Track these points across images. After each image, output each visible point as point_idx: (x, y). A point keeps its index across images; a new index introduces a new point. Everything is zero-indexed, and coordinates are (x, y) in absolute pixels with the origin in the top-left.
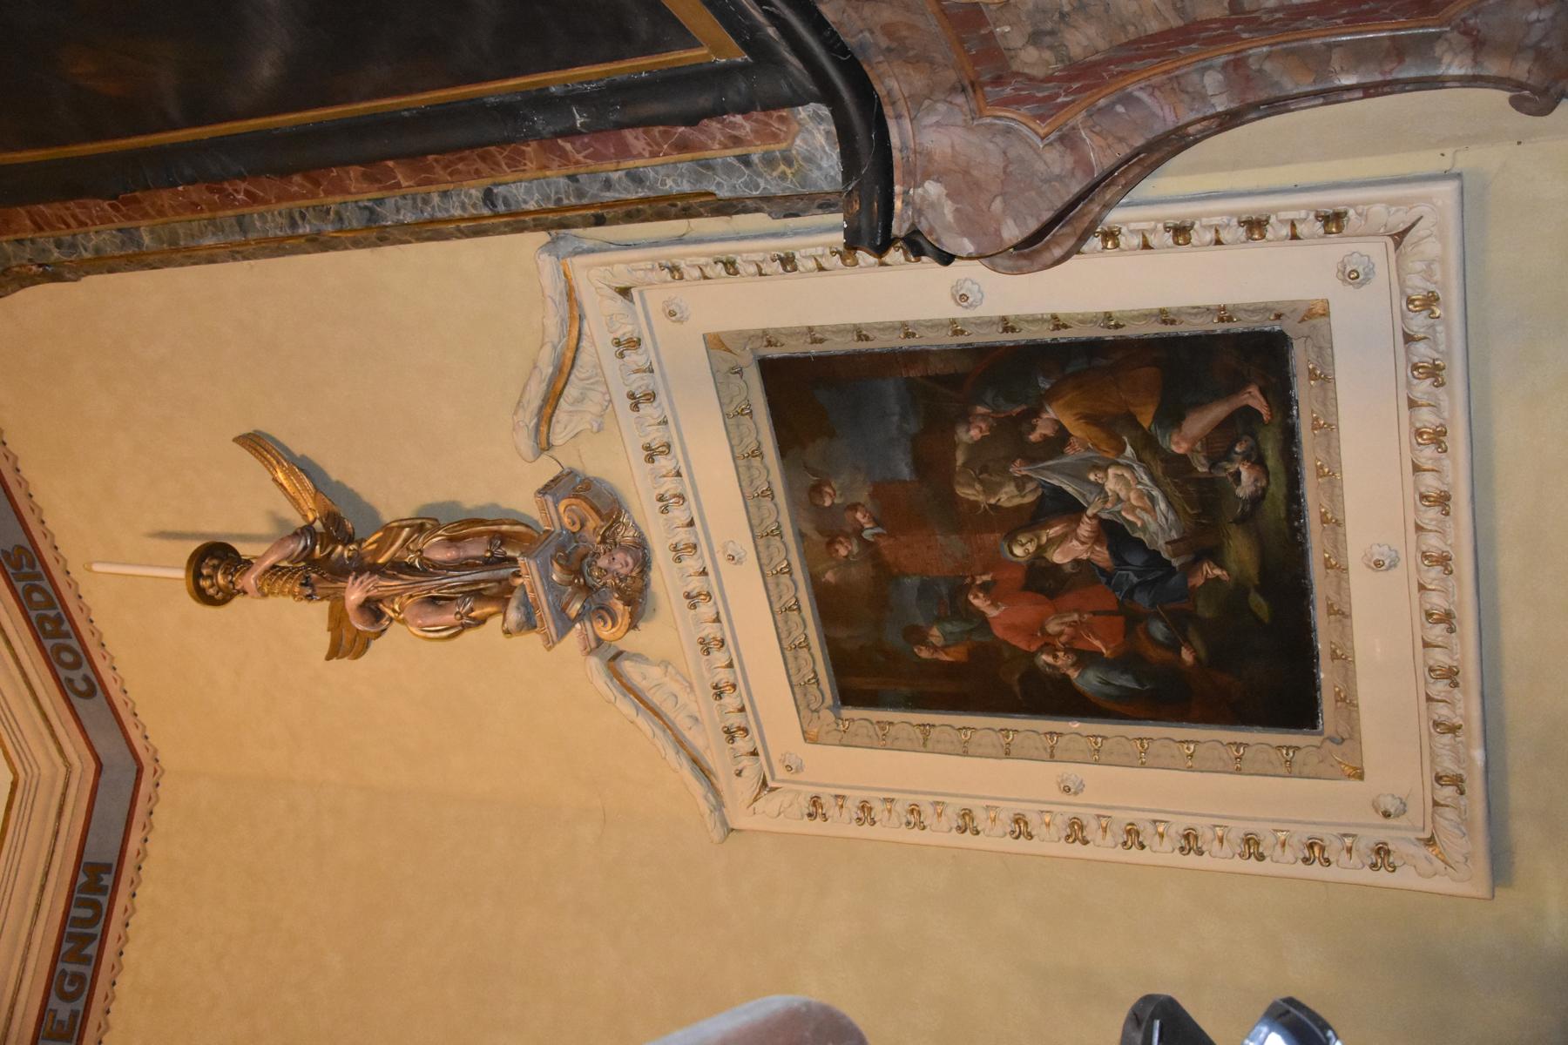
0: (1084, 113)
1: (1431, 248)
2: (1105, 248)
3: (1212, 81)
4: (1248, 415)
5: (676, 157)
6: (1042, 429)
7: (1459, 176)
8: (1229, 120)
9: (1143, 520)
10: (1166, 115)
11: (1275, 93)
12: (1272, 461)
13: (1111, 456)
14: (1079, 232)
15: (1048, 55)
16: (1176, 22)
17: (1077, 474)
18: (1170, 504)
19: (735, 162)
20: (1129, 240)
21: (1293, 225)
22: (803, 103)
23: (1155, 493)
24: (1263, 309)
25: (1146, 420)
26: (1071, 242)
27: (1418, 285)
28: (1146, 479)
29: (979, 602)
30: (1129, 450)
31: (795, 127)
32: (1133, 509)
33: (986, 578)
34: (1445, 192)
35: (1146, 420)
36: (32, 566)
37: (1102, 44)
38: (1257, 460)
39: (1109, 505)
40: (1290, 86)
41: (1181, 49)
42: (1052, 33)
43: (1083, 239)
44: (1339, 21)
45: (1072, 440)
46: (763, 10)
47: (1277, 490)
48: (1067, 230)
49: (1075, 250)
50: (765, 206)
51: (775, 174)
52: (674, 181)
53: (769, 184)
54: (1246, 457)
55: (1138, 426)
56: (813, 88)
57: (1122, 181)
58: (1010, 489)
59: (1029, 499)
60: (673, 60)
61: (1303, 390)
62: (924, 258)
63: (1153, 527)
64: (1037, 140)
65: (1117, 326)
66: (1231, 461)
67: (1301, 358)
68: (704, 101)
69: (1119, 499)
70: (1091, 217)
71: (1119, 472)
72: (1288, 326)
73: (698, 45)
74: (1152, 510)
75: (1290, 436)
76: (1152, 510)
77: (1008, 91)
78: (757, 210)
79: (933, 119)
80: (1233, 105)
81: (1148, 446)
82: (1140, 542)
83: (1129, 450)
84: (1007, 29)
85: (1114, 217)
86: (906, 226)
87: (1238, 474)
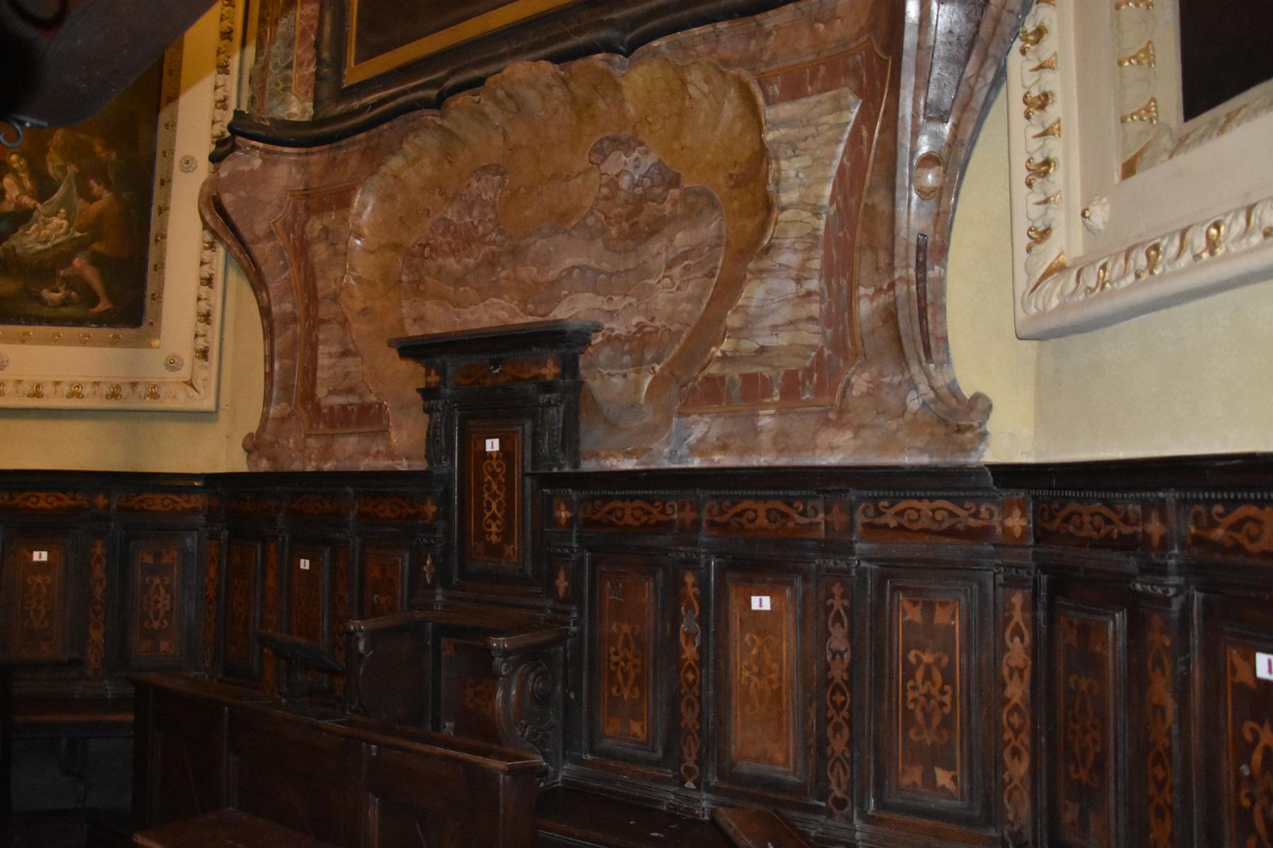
0: (282, 245)
1: (181, 396)
2: (204, 242)
3: (288, 307)
4: (94, 300)
5: (298, 28)
6: (96, 188)
7: (216, 412)
8: (265, 312)
9: (30, 235)
10: (275, 284)
11: (277, 331)
12: (64, 310)
13: (76, 223)
14: (218, 231)
15: (315, 234)
16: (320, 294)
17: (65, 202)
18: (40, 252)
19: (289, 60)
20: (207, 255)
21: (203, 336)
22: (314, 107)
23: (49, 245)
24: (158, 316)
25: (97, 246)
26: (212, 224)
27: (163, 391)
28: (58, 241)
30: (78, 234)
31: (302, 99)
32: (38, 230)
34: (209, 404)
35: (97, 246)
37: (316, 260)
38: (65, 303)
39: (42, 217)
40: (277, 342)
41: (306, 295)
42: (327, 238)
43: (213, 232)
44: (306, 365)
45: (88, 204)
46: (368, 106)
47: (45, 311)
48: (220, 225)
49: (206, 226)
50: (259, 66)
51: (279, 81)
52: (285, 24)
53: (274, 75)
54: (67, 297)
55: (94, 241)
56: (321, 115)
57: (242, 257)
59: (51, 171)
60: (1198, 603)
61: (107, 332)
62: (214, 147)
63: (25, 240)
64: (273, 220)
65: (157, 241)
66: (66, 289)
67: (125, 332)
68: (326, 55)
69: (46, 223)
70: (225, 238)
71: (64, 226)
72: (144, 327)
73: (356, 63)
74: (37, 241)
75: (79, 322)
76: (37, 241)
77: (301, 211)
78: (256, 61)
79: (294, 170)
80: (274, 314)
81: (79, 246)
82: (15, 230)
83: (78, 234)
84: (333, 218)
85: (221, 250)
86: (240, 145)
87: (57, 291)
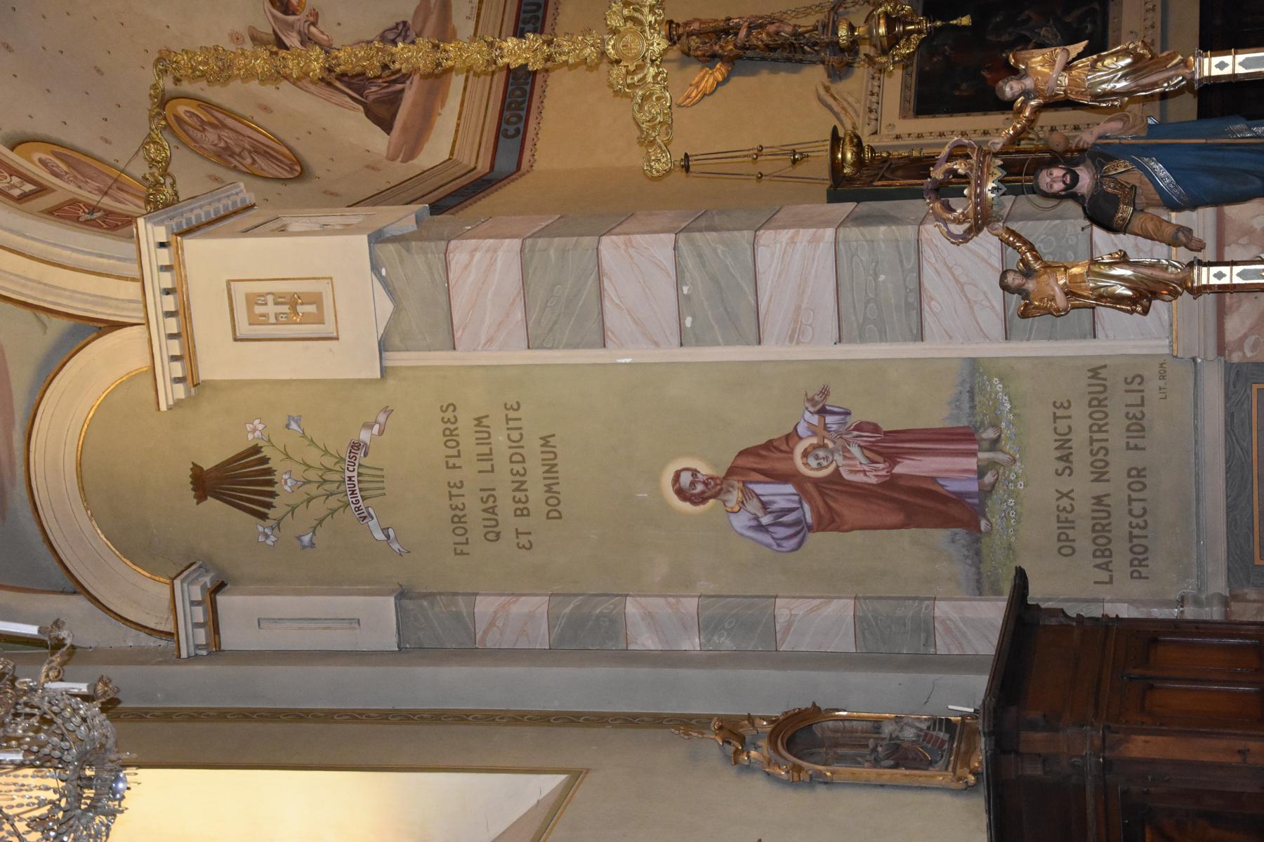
6: (1023, 17)
29: (984, 73)
32: (1049, 39)
33: (990, 65)
36: (513, 91)
58: (1007, 35)
